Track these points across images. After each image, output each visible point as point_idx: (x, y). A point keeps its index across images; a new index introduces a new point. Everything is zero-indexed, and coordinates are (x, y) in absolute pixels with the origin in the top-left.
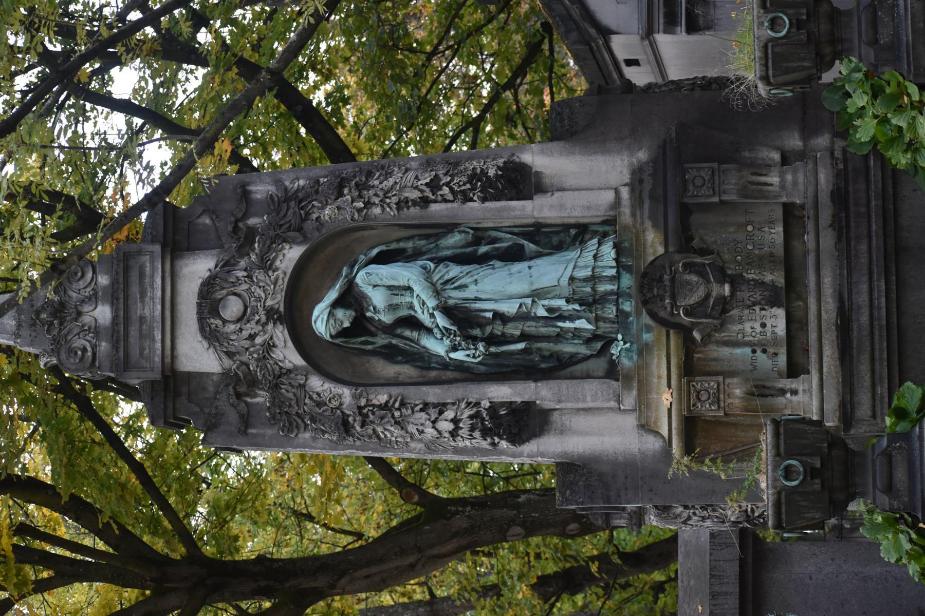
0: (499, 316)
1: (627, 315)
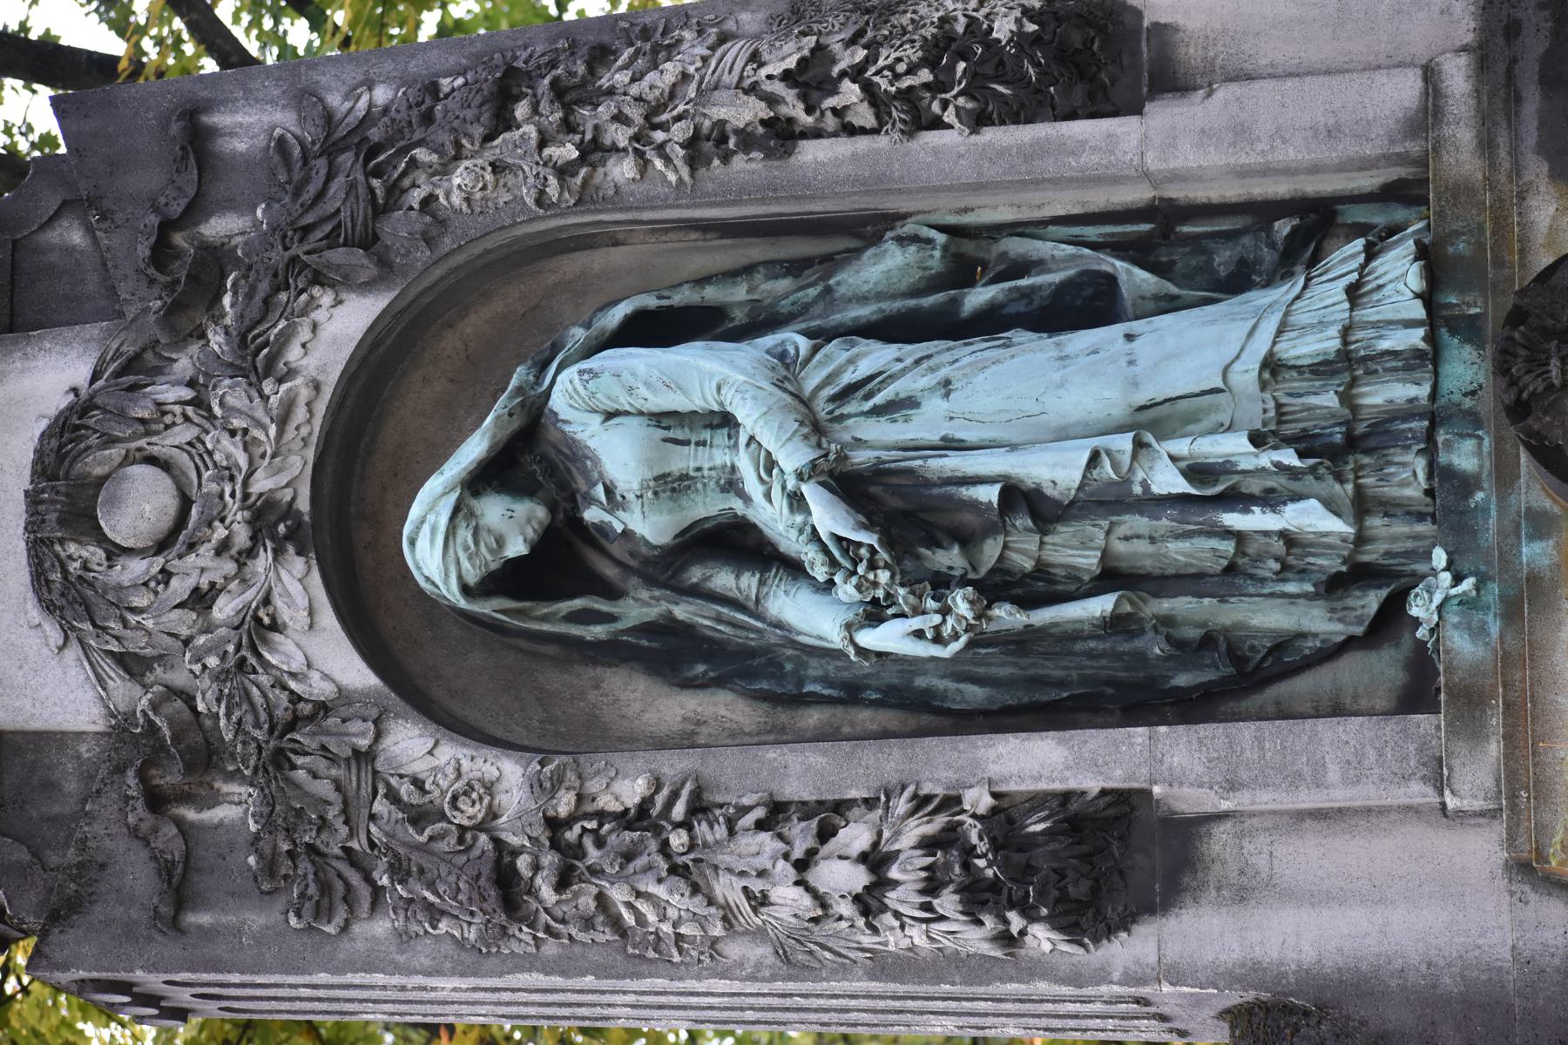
0: (1016, 496)
1: (1465, 484)
